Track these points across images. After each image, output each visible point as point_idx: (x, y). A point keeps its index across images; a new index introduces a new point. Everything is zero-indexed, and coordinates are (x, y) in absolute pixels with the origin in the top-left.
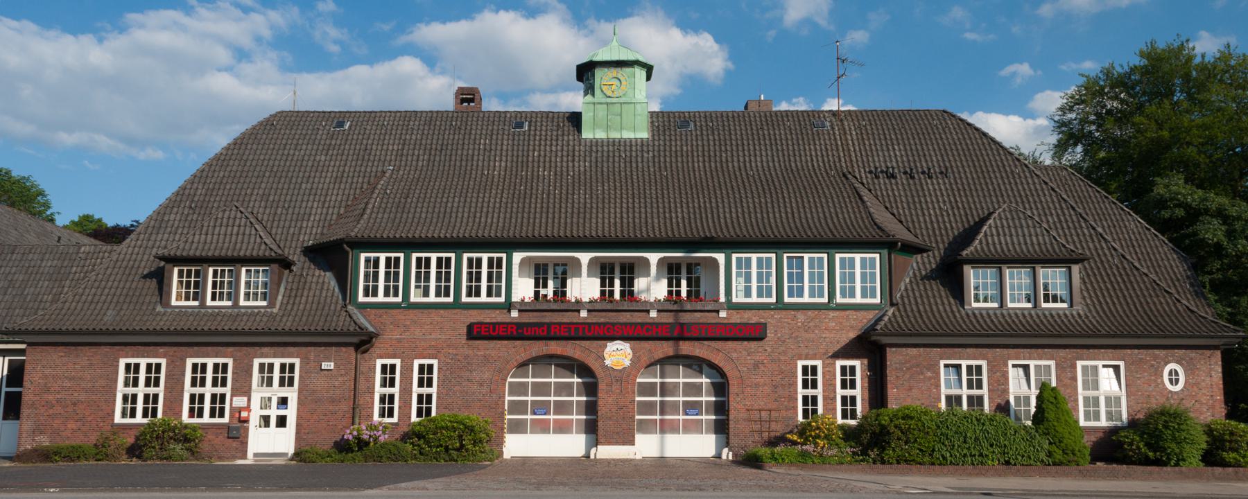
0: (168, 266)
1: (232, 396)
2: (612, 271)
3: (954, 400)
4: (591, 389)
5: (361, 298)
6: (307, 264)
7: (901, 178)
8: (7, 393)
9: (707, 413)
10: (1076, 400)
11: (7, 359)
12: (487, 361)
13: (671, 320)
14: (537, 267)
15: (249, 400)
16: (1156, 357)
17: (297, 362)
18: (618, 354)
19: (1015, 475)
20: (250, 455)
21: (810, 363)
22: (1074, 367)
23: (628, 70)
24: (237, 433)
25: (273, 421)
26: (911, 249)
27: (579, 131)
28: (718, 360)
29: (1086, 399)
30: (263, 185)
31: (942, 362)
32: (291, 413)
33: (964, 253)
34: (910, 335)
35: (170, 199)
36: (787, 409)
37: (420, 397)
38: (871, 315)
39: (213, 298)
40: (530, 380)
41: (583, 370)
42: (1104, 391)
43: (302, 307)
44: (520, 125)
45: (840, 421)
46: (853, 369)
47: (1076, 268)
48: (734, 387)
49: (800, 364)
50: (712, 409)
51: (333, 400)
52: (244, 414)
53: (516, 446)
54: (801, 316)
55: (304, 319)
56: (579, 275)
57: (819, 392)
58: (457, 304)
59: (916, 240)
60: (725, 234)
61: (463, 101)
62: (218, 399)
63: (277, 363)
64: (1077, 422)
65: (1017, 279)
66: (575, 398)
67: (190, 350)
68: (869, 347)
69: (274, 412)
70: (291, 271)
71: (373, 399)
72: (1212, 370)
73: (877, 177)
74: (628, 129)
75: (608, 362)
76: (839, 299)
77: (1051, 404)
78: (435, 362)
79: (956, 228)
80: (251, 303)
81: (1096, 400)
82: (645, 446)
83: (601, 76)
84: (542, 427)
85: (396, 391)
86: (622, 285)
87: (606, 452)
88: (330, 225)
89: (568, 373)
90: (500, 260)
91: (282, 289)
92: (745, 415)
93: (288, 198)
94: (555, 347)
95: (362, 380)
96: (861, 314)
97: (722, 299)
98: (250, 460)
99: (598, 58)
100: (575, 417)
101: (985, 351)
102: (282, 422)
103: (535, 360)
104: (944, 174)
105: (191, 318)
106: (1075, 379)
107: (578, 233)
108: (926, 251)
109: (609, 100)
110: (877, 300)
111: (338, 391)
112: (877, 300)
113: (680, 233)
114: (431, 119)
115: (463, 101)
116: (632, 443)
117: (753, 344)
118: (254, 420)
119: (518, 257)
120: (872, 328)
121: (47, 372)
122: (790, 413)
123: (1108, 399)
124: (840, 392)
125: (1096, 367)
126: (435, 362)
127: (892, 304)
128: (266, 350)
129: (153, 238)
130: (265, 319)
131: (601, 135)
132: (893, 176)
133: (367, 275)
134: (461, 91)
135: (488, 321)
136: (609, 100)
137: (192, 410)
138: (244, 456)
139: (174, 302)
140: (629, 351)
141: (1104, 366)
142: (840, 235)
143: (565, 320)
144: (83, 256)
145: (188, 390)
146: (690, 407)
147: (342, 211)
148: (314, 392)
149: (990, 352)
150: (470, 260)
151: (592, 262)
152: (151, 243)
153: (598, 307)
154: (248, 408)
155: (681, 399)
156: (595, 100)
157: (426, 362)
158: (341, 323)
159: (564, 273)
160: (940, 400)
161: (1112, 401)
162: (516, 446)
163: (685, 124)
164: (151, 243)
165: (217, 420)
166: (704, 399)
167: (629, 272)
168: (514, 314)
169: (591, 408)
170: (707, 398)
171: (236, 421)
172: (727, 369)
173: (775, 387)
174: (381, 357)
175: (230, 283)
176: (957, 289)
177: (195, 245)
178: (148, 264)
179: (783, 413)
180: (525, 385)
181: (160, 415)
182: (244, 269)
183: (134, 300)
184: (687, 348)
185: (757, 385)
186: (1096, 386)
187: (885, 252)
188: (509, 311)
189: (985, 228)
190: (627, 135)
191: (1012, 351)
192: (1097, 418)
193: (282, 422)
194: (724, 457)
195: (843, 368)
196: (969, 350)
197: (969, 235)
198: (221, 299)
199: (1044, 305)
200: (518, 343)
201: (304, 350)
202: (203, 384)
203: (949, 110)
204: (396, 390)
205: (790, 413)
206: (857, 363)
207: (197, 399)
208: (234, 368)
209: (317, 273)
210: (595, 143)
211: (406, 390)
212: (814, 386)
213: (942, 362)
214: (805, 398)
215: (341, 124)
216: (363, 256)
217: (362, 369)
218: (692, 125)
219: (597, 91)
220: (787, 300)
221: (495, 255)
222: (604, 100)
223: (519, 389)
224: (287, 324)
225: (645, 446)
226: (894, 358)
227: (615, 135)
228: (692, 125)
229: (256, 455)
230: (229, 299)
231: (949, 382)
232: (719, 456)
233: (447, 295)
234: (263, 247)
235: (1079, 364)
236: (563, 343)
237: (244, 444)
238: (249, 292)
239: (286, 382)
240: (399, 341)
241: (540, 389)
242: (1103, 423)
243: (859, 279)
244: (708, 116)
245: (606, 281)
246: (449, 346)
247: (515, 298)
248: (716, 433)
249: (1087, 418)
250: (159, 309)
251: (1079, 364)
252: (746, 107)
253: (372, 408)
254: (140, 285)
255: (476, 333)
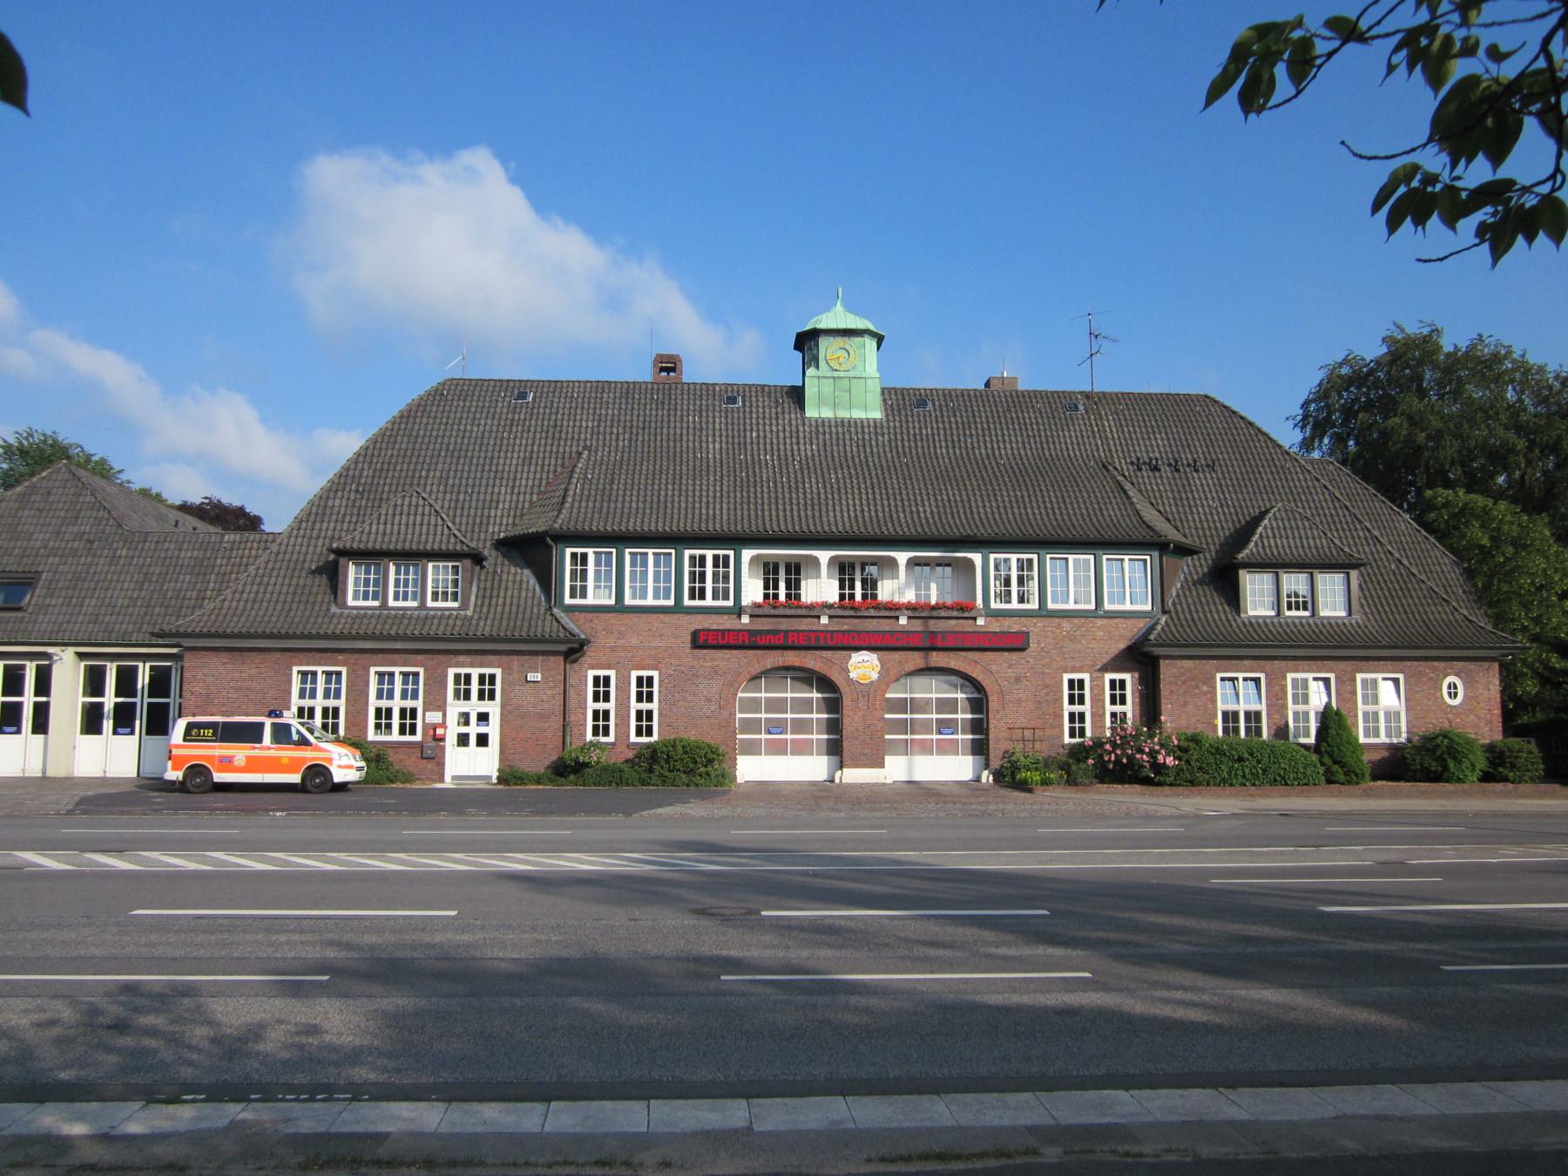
0: (342, 561)
1: (425, 711)
2: (776, 572)
3: (1230, 717)
4: (833, 705)
5: (568, 600)
6: (500, 560)
7: (1166, 471)
8: (149, 704)
9: (963, 732)
10: (1356, 716)
11: (148, 665)
12: (715, 672)
13: (920, 629)
14: (766, 565)
15: (444, 716)
16: (1435, 670)
17: (498, 672)
18: (864, 666)
19: (1298, 796)
20: (448, 778)
21: (1076, 676)
22: (1354, 680)
23: (857, 340)
24: (431, 750)
25: (473, 740)
26: (1183, 551)
27: (802, 408)
28: (976, 673)
29: (1366, 714)
30: (440, 467)
31: (1219, 676)
32: (493, 730)
33: (1240, 556)
34: (1186, 646)
35: (331, 481)
36: (1052, 727)
37: (596, 713)
38: (1141, 625)
39: (396, 598)
40: (763, 695)
41: (825, 683)
42: (1384, 706)
43: (499, 609)
44: (732, 400)
45: (1067, 740)
46: (1122, 682)
47: (1354, 574)
48: (994, 704)
49: (1066, 677)
50: (968, 727)
51: (542, 717)
52: (440, 731)
53: (750, 769)
54: (1065, 624)
55: (504, 623)
56: (818, 576)
57: (1087, 708)
58: (678, 608)
59: (1183, 540)
60: (983, 532)
61: (662, 369)
62: (408, 714)
63: (475, 673)
64: (1357, 739)
65: (1295, 582)
66: (815, 716)
67: (374, 657)
68: (1141, 658)
69: (473, 730)
70: (482, 567)
71: (585, 715)
72: (1491, 684)
73: (1140, 469)
74: (858, 408)
75: (852, 675)
76: (1107, 606)
77: (1332, 723)
78: (655, 674)
79: (1228, 528)
80: (401, 604)
81: (1376, 714)
82: (895, 769)
83: (826, 346)
84: (778, 749)
85: (617, 707)
86: (788, 587)
87: (852, 776)
88: (522, 515)
89: (806, 687)
90: (726, 558)
91: (474, 589)
92: (1006, 734)
93: (471, 482)
94: (792, 658)
95: (571, 693)
96: (1131, 622)
97: (979, 602)
98: (448, 783)
99: (822, 326)
100: (815, 736)
101: (1262, 663)
102: (483, 740)
103: (767, 673)
104: (1211, 467)
105: (374, 621)
106: (1354, 693)
107: (815, 528)
108: (1196, 553)
109: (836, 374)
110: (1148, 607)
111: (546, 706)
112: (1148, 607)
113: (932, 531)
114: (628, 391)
115: (662, 369)
116: (882, 765)
117: (1014, 656)
118: (451, 739)
119: (747, 554)
120: (1144, 638)
121: (209, 680)
122: (1055, 732)
123: (1387, 714)
124: (634, 706)
125: (1375, 681)
126: (655, 674)
127: (1164, 612)
128: (462, 658)
129: (317, 526)
130: (459, 623)
131: (827, 413)
132: (1156, 469)
133: (573, 572)
134: (660, 358)
135: (714, 627)
136: (836, 374)
137: (378, 726)
138: (442, 780)
139: (351, 602)
140: (876, 662)
141: (1315, 679)
142: (1108, 535)
143: (803, 627)
144: (228, 546)
145: (373, 703)
146: (943, 726)
147: (535, 498)
148: (518, 707)
149: (1268, 664)
150: (692, 558)
151: (832, 560)
152: (315, 533)
153: (760, 612)
154: (443, 725)
155: (935, 716)
156: (820, 373)
157: (645, 673)
158: (547, 628)
159: (798, 572)
160: (1215, 716)
161: (1392, 716)
162: (750, 769)
163: (922, 403)
164: (315, 533)
165: (408, 738)
166: (960, 716)
167: (795, 571)
168: (745, 619)
169: (834, 727)
170: (964, 716)
171: (430, 739)
172: (986, 683)
173: (1039, 702)
174: (593, 668)
175: (415, 581)
176: (1233, 596)
177: (372, 537)
178: (316, 554)
179: (1049, 732)
180: (757, 701)
181: (1088, 733)
182: (430, 565)
183: (304, 598)
184: (938, 659)
185: (1019, 701)
186: (1306, 701)
187: (1156, 554)
188: (739, 616)
189: (1260, 529)
190: (858, 414)
191: (1290, 663)
192: (1377, 735)
193: (483, 740)
194: (984, 780)
195: (1113, 682)
196: (1246, 662)
197: (1243, 535)
198: (405, 599)
199: (1288, 613)
200: (735, 652)
201: (505, 658)
202: (313, 695)
203: (1211, 394)
204: (611, 706)
205: (1055, 732)
206: (1127, 677)
207: (384, 714)
208: (426, 679)
209: (513, 570)
210: (821, 423)
211: (623, 705)
212: (1082, 702)
213: (1219, 676)
214: (1072, 715)
215: (523, 396)
216: (569, 551)
217: (572, 680)
218: (930, 404)
219: (822, 363)
220: (1050, 606)
221: (721, 552)
222: (830, 374)
223: (754, 705)
224: (486, 629)
225: (895, 769)
226: (1167, 671)
227: (843, 414)
228: (930, 404)
229: (454, 778)
230: (414, 599)
231: (1236, 694)
232: (978, 780)
233: (726, 598)
234: (453, 540)
235: (1359, 677)
236: (803, 653)
237: (441, 765)
238: (434, 590)
239: (487, 695)
240: (613, 649)
241: (774, 705)
242: (1383, 738)
243: (1129, 584)
244: (948, 395)
245: (845, 582)
246: (671, 656)
247: (746, 601)
248: (973, 754)
249: (1367, 735)
250: (334, 609)
251: (1359, 677)
252: (987, 384)
253: (585, 724)
254: (309, 582)
255: (701, 641)
